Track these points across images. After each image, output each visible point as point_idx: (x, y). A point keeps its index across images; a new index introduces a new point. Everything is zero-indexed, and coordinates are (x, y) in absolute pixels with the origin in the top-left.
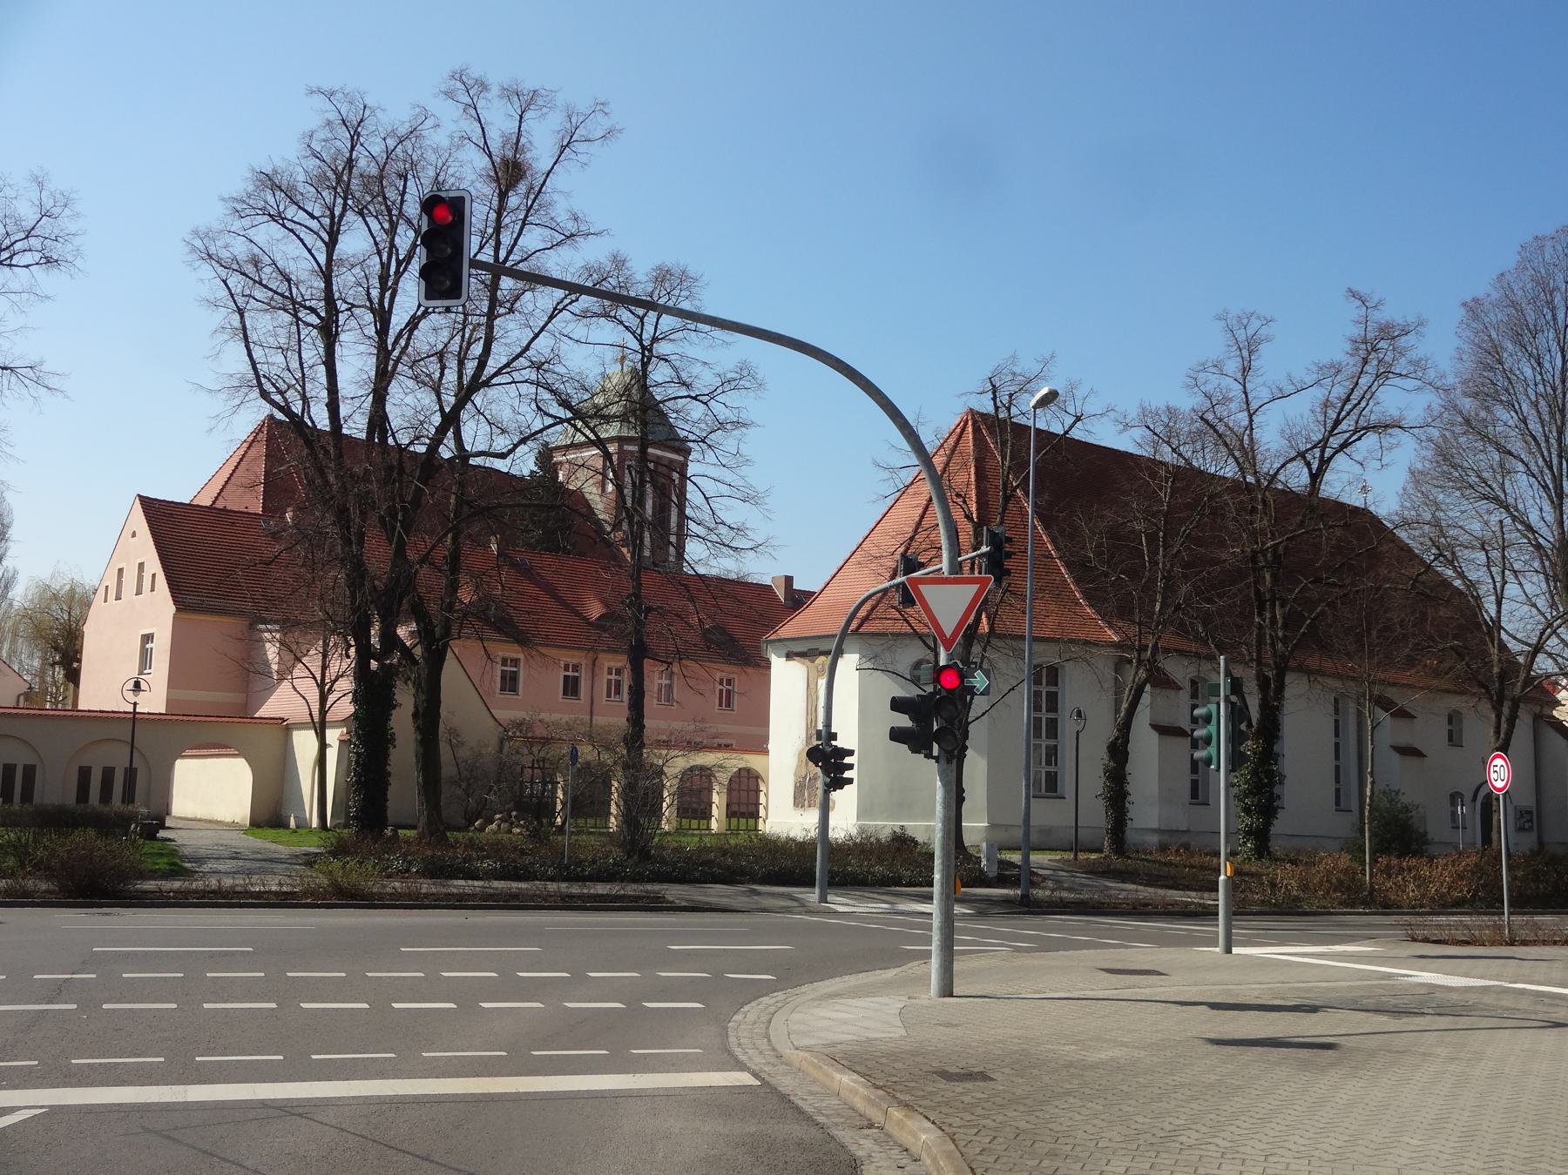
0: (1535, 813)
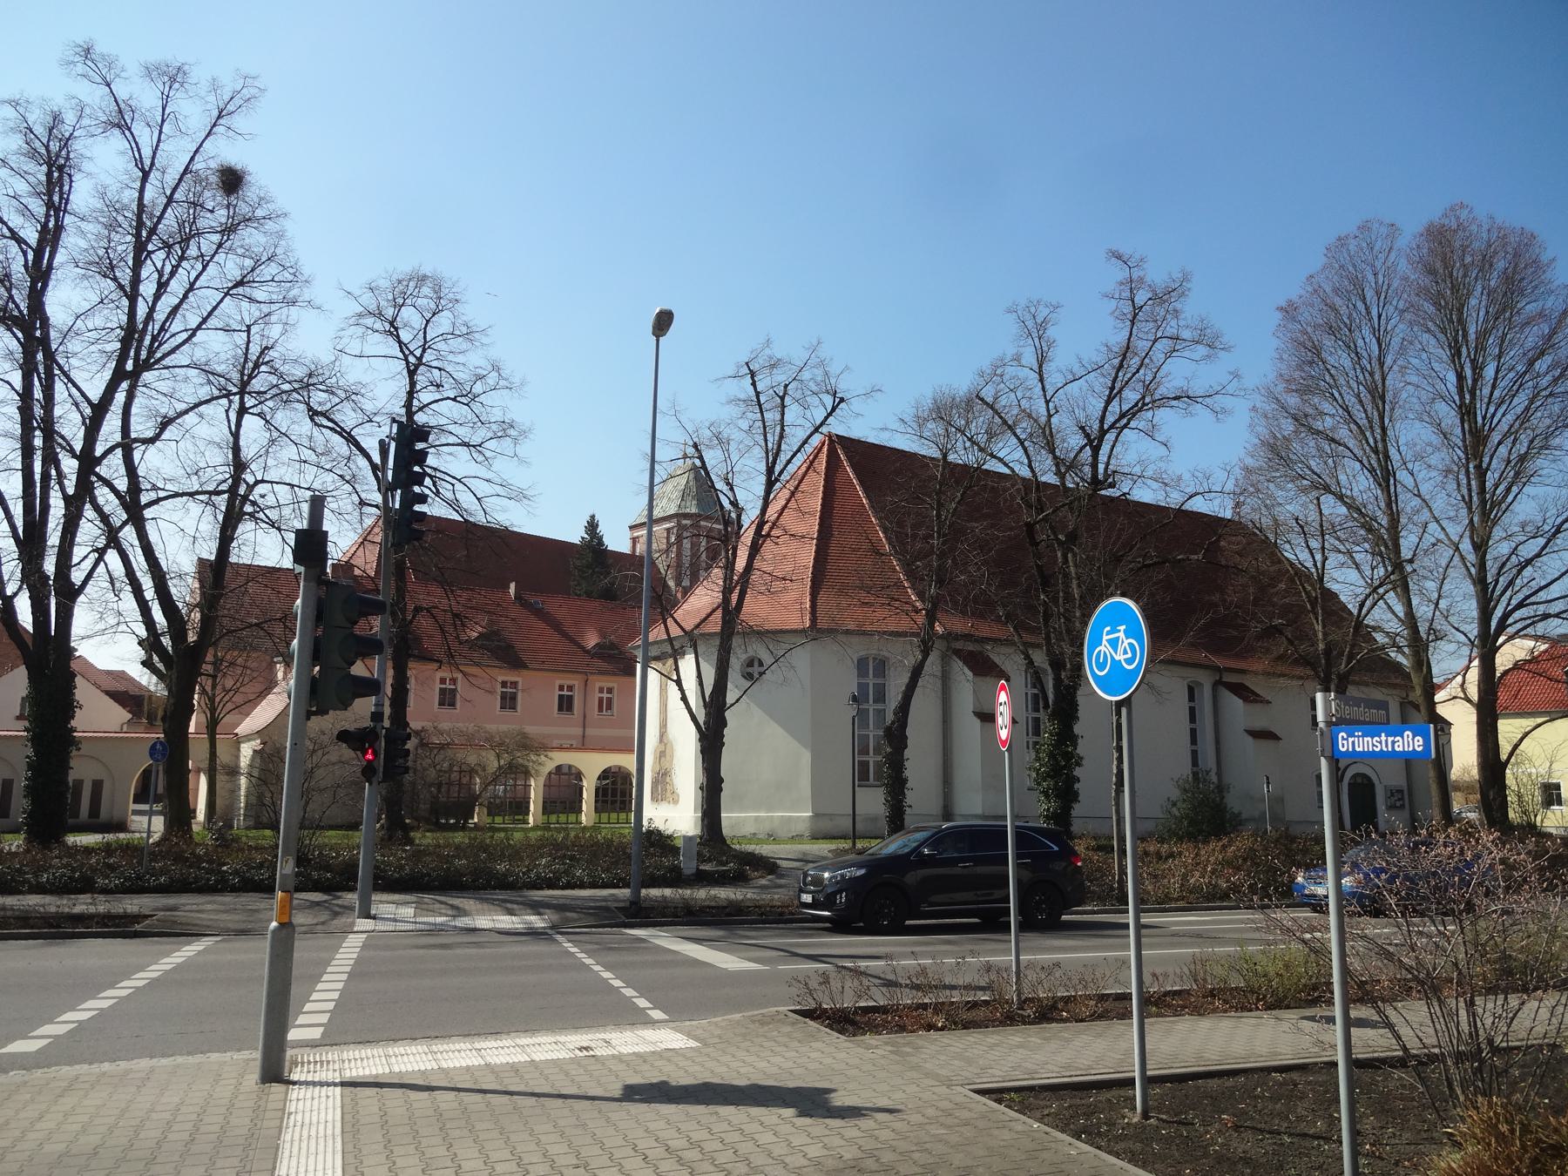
0: (1406, 792)
